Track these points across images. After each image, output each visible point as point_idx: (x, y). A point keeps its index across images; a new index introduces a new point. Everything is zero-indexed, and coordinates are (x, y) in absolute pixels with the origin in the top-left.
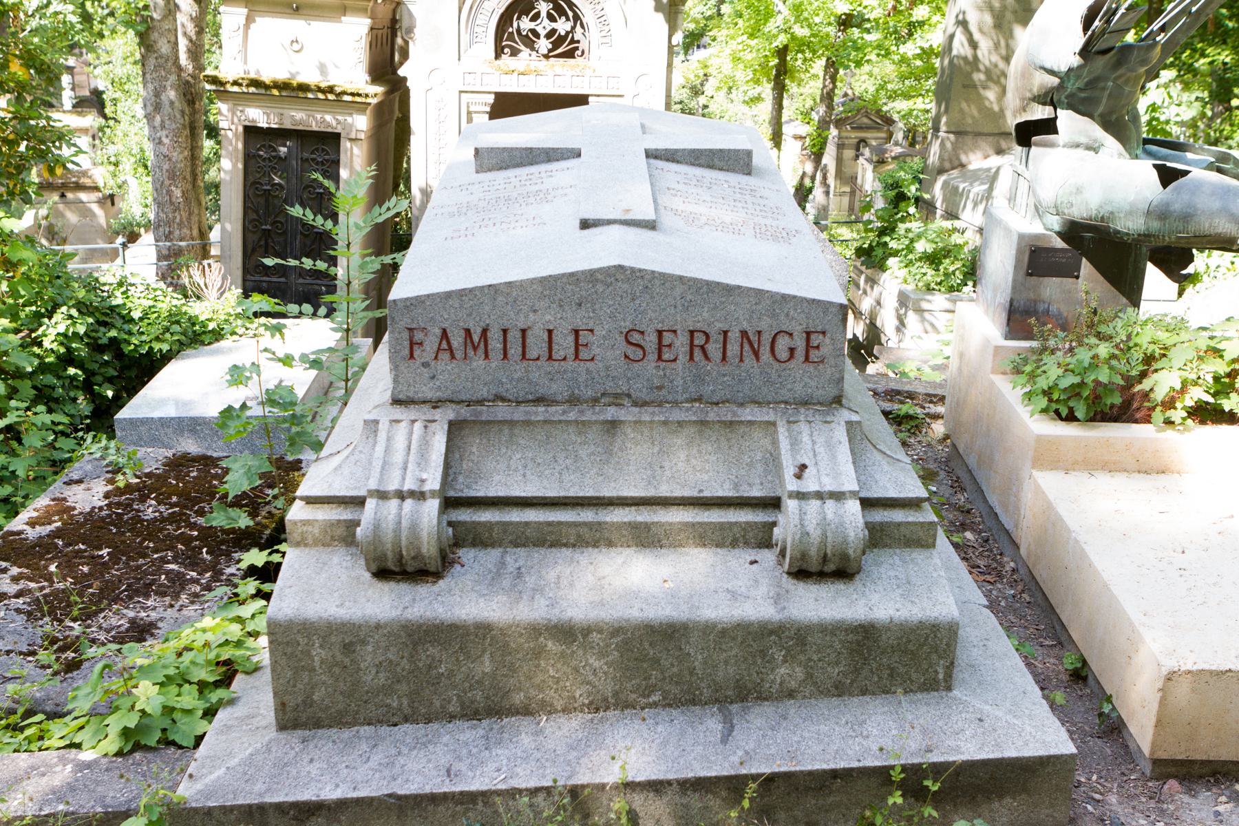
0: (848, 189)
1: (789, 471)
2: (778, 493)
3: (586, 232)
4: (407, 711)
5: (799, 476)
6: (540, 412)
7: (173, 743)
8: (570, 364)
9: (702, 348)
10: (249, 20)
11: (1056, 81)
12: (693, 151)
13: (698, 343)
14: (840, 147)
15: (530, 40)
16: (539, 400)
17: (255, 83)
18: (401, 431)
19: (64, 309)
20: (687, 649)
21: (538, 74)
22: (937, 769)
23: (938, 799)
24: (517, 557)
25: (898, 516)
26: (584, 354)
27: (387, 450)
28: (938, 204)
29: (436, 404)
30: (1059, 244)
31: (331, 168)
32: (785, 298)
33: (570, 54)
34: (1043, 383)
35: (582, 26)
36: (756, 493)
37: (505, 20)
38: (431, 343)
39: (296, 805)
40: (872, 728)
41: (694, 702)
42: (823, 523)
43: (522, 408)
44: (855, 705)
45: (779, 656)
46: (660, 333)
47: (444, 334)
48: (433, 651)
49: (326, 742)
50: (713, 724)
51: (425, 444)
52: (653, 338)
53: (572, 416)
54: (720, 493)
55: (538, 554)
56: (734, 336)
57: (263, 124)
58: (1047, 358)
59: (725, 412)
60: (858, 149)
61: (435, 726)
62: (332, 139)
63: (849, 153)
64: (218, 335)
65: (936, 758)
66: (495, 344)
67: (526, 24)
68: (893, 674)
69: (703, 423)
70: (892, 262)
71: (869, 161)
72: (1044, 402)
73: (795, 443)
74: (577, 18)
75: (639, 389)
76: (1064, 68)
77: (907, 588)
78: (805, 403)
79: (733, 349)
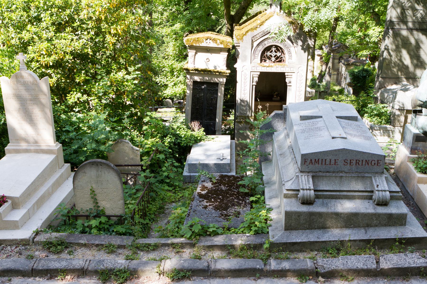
0: (336, 73)
1: (376, 186)
2: (373, 190)
3: (334, 139)
4: (308, 227)
5: (377, 187)
6: (328, 174)
7: (264, 233)
8: (334, 166)
9: (358, 163)
10: (196, 53)
11: (422, 103)
12: (345, 116)
13: (357, 162)
14: (334, 59)
15: (269, 58)
16: (327, 172)
17: (196, 70)
18: (303, 178)
19: (169, 135)
20: (358, 217)
21: (272, 67)
22: (404, 239)
23: (404, 244)
24: (326, 201)
25: (395, 194)
26: (336, 164)
27: (302, 181)
28: (379, 98)
29: (308, 172)
30: (422, 135)
31: (216, 92)
32: (374, 154)
33: (280, 61)
34: (419, 166)
35: (284, 54)
36: (369, 190)
37: (263, 53)
38: (308, 162)
39: (292, 243)
40: (392, 232)
41: (359, 227)
42: (383, 195)
43: (324, 173)
44: (388, 228)
45: (375, 219)
46: (351, 160)
47: (311, 160)
48: (313, 217)
49: (295, 233)
50: (363, 231)
51: (308, 181)
52: (349, 161)
53: (334, 175)
54: (362, 190)
55: (329, 200)
56: (364, 161)
57: (199, 80)
58: (420, 160)
59: (362, 175)
60: (339, 60)
61: (313, 230)
62: (216, 84)
63: (336, 61)
64: (200, 140)
65: (404, 237)
66: (320, 162)
67: (269, 54)
68: (395, 222)
69: (358, 177)
70: (366, 115)
71: (344, 64)
72: (420, 170)
73: (376, 181)
74: (282, 52)
75: (346, 170)
76: (424, 101)
77: (398, 207)
78: (377, 173)
79: (364, 163)
